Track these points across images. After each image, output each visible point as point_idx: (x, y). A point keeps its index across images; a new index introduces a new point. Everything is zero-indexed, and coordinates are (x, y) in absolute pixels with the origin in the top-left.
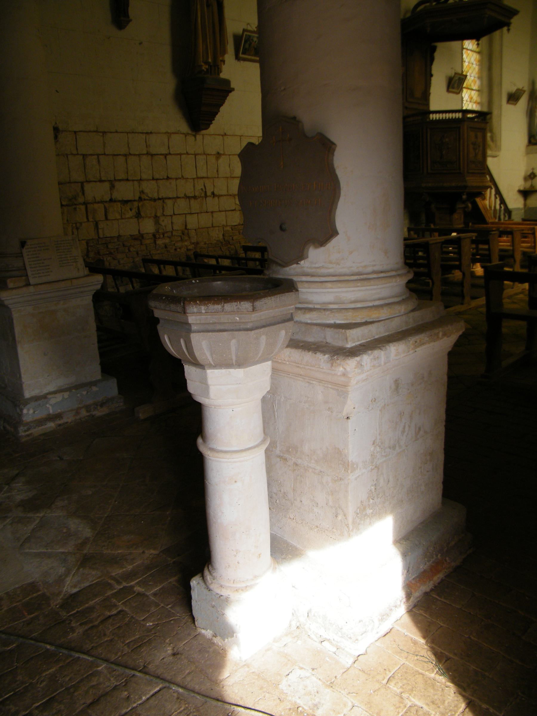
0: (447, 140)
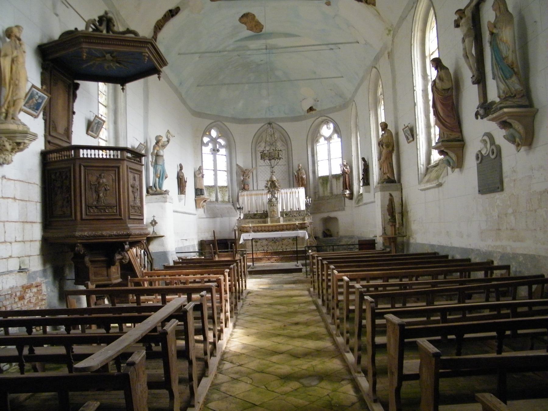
0: (105, 180)
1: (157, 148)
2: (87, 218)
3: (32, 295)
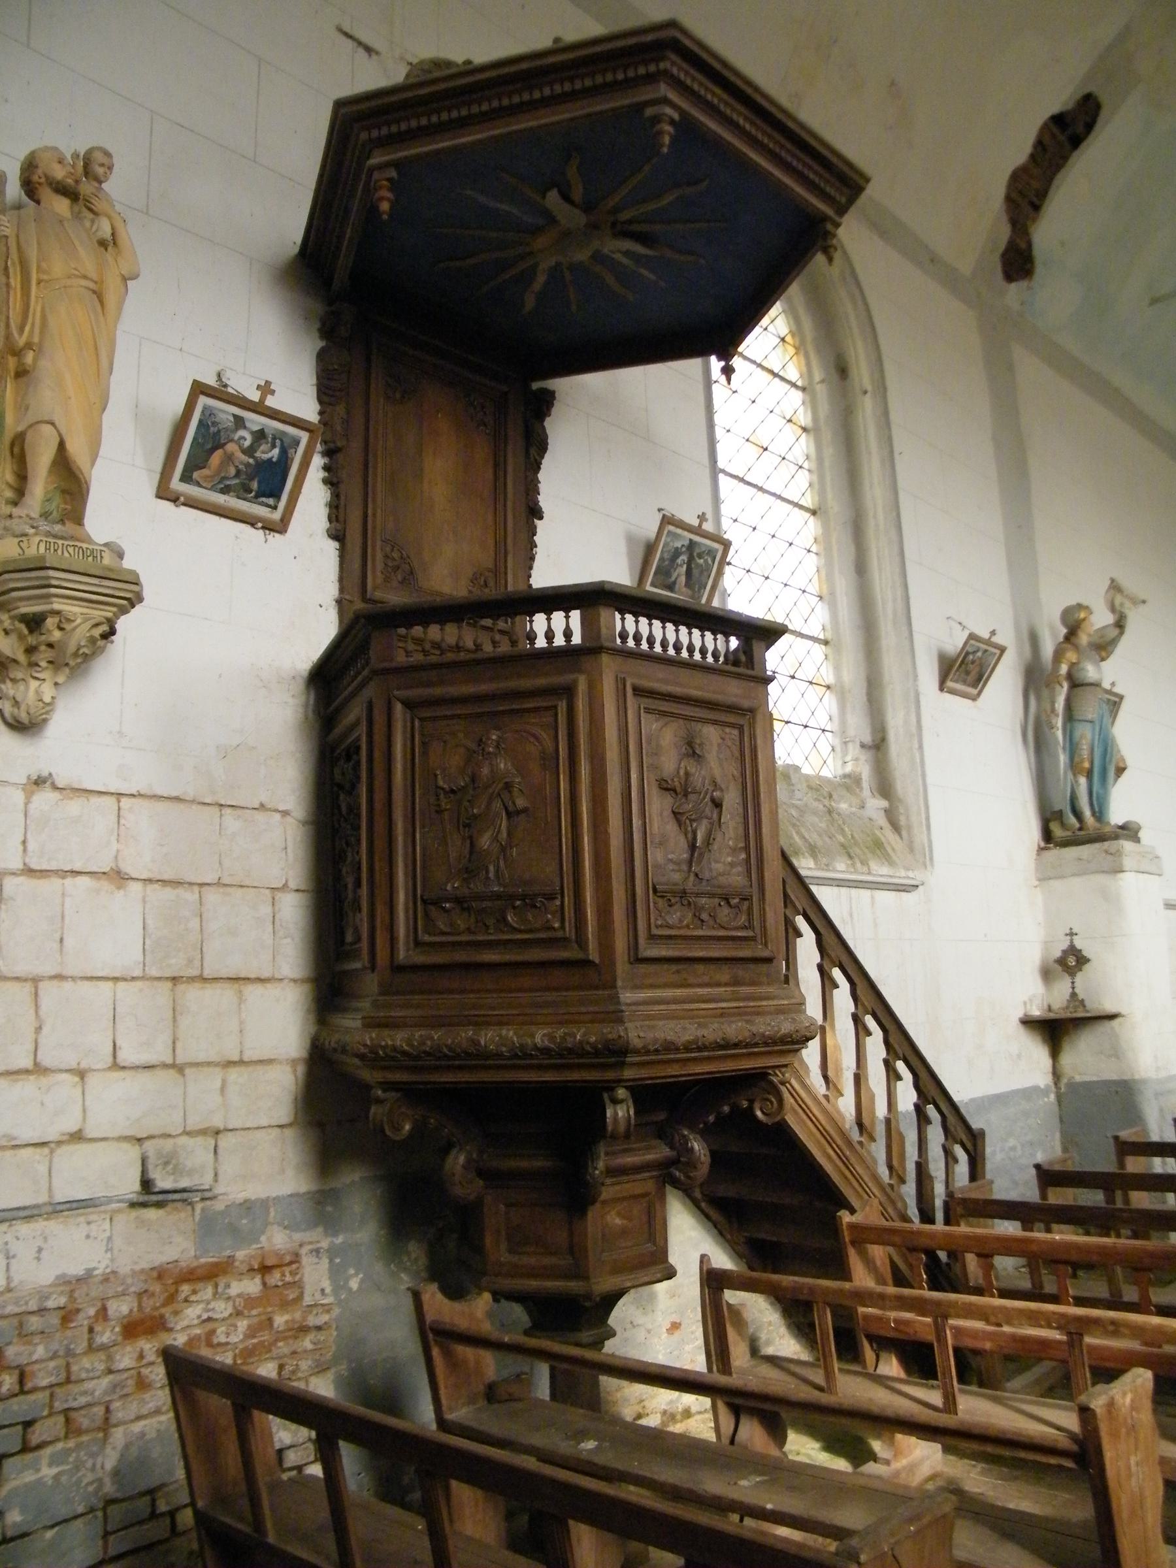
1: (1071, 656)
2: (420, 959)
3: (222, 1309)
